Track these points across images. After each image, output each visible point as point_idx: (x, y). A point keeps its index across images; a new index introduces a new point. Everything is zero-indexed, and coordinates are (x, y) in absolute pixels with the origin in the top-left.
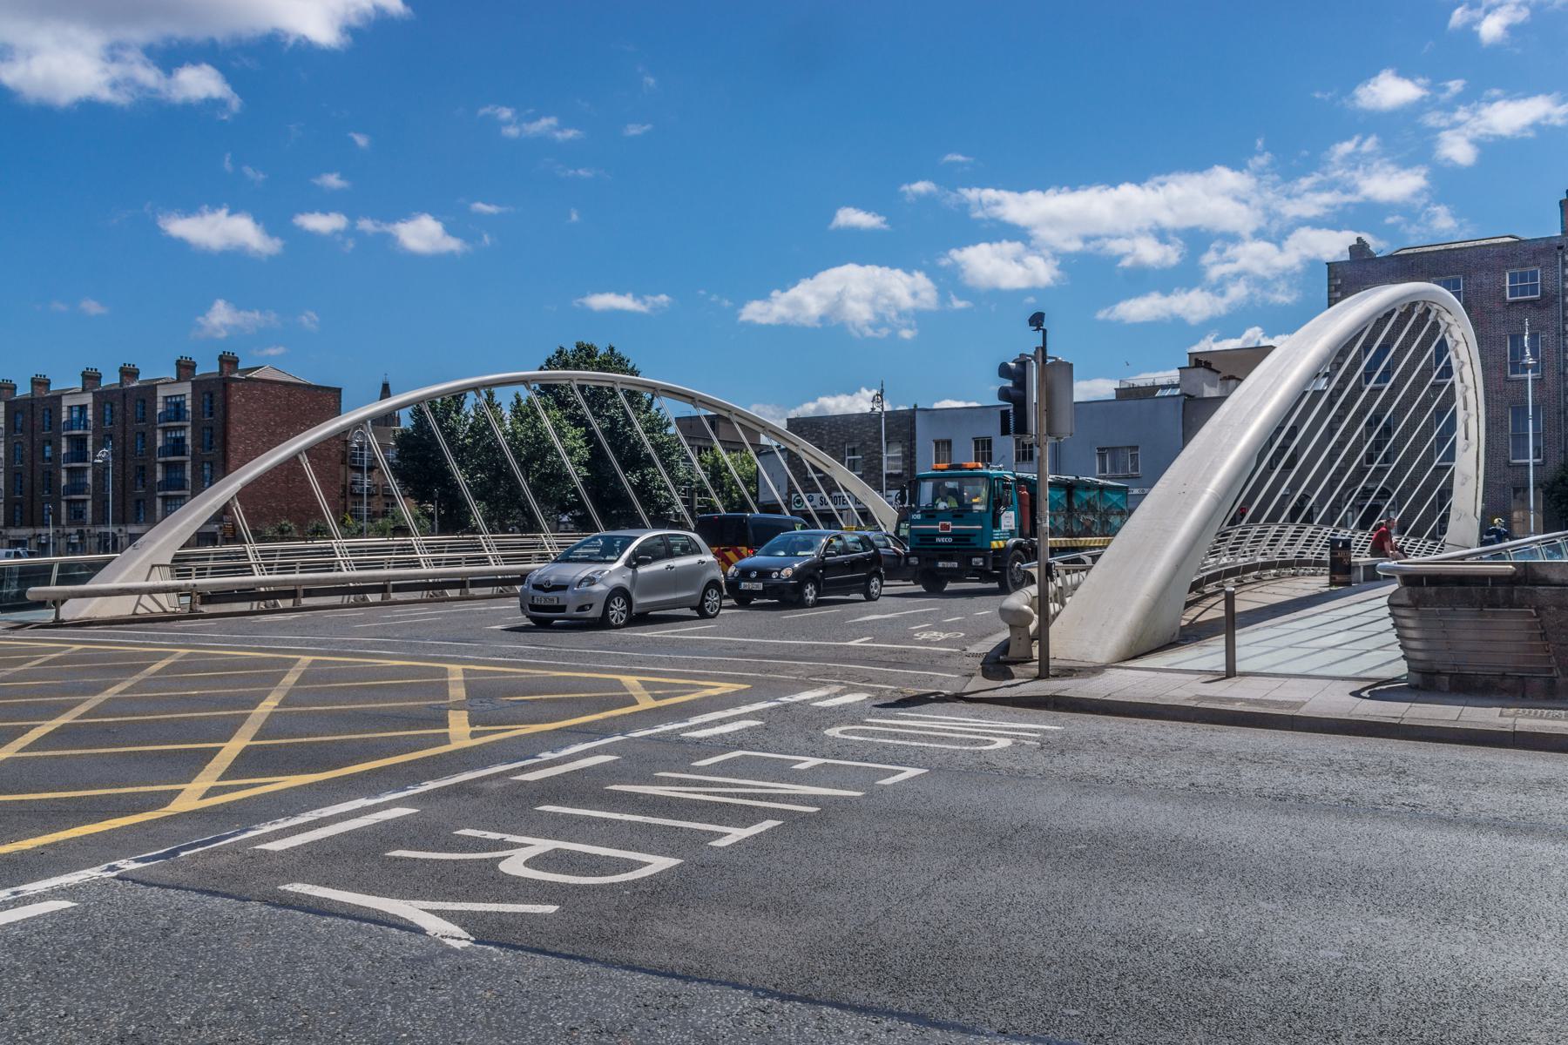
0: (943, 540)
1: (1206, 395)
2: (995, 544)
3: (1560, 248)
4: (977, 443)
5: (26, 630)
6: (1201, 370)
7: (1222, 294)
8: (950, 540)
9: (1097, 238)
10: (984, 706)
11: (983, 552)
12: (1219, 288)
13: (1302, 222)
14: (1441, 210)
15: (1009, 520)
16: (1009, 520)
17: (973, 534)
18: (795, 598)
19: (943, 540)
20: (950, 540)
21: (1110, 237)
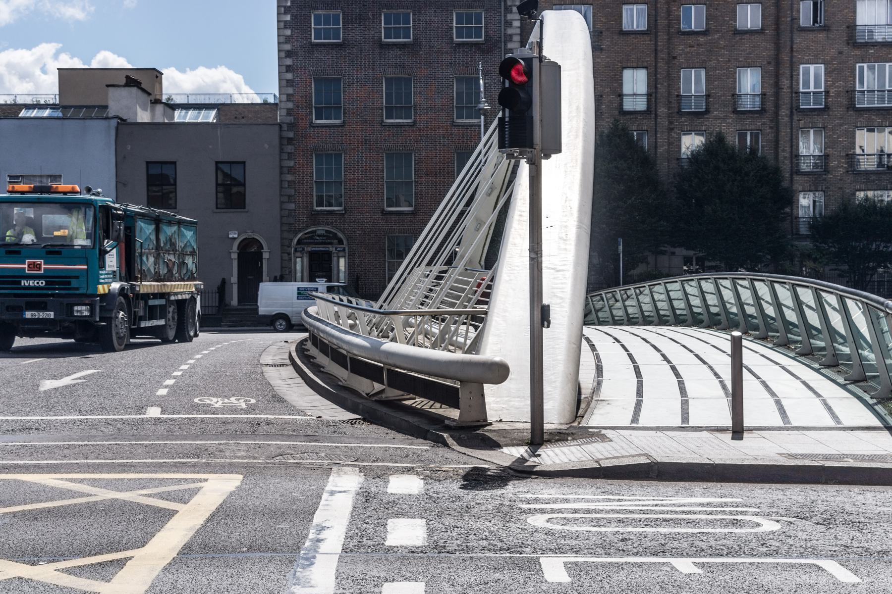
1: (139, 120)
2: (102, 289)
5: (34, 434)
6: (134, 90)
8: (42, 283)
10: (569, 480)
11: (89, 298)
15: (112, 261)
16: (112, 261)
17: (76, 276)
20: (42, 283)
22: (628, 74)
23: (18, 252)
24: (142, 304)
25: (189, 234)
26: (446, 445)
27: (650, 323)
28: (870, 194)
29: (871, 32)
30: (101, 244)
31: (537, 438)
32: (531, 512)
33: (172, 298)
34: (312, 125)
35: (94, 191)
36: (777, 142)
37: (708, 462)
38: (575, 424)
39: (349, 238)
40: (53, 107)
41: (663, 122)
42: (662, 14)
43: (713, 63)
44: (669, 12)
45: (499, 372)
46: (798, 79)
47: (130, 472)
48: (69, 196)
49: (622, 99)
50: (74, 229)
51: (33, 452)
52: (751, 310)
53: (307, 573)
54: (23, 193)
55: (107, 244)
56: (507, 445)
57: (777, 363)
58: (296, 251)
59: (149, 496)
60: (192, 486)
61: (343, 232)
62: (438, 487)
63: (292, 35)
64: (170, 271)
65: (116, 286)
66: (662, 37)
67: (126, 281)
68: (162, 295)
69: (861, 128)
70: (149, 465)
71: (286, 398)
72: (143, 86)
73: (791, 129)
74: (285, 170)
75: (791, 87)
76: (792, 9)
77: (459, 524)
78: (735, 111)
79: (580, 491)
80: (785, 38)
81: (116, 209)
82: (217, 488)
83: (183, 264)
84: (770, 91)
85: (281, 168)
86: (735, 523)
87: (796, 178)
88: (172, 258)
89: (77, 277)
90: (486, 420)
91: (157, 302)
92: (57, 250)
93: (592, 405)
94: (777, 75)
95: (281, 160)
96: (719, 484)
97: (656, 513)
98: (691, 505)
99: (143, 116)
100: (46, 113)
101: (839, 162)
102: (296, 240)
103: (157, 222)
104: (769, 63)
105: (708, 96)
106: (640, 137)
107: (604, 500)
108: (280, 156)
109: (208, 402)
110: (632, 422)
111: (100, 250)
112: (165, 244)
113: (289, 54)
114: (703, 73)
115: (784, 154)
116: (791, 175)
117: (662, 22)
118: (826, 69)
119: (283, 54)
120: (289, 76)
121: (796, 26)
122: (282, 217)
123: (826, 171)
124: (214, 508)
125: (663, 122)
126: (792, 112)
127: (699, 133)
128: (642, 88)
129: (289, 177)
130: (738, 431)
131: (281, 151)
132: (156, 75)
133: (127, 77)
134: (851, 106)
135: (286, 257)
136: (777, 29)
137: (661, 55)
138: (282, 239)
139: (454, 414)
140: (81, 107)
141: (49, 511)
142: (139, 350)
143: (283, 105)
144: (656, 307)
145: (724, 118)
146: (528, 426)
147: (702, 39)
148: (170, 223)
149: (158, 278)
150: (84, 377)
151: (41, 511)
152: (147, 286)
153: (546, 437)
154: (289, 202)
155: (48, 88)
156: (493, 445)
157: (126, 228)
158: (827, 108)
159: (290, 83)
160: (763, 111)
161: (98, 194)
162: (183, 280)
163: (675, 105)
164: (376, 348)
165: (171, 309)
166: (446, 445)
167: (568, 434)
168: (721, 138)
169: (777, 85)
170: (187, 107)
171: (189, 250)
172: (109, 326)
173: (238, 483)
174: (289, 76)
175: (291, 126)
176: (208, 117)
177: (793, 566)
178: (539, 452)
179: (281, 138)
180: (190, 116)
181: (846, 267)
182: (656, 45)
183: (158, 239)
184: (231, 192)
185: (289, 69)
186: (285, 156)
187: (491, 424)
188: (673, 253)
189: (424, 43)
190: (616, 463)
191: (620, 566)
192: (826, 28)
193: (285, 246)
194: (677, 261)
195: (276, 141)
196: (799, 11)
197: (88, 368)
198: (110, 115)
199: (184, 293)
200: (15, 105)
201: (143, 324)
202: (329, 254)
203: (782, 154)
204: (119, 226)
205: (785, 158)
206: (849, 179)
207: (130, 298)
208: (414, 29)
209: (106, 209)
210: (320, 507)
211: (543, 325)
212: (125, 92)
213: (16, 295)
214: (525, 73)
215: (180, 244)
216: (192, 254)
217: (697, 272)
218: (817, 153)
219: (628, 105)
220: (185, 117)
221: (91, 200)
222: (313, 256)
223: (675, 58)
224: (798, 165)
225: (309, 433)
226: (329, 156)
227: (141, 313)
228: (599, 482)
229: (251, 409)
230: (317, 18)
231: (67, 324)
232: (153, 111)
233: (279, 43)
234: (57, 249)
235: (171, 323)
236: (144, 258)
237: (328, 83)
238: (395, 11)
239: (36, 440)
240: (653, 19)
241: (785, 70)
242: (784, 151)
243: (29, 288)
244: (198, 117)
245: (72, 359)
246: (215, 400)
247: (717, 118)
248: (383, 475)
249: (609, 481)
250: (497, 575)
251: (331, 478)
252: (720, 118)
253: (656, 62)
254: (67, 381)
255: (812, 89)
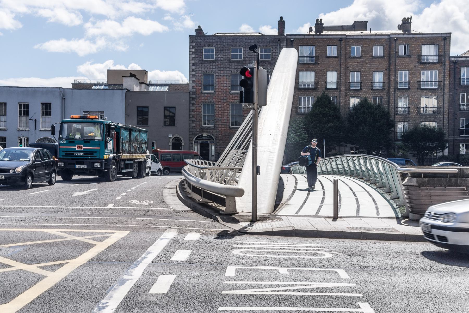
0: (78, 154)
1: (135, 90)
2: (105, 157)
3: (279, 40)
4: (20, 105)
5: (59, 213)
6: (133, 78)
7: (94, 43)
8: (82, 154)
9: (35, 7)
10: (259, 236)
11: (100, 160)
12: (93, 40)
13: (131, 14)
14: (188, 18)
15: (110, 146)
16: (110, 146)
17: (95, 151)
18: (23, 183)
19: (78, 154)
20: (82, 154)
21: (40, 8)
22: (329, 74)
23: (73, 142)
24: (122, 163)
25: (144, 135)
26: (218, 221)
27: (324, 174)
28: (427, 123)
29: (427, 58)
30: (106, 139)
31: (254, 219)
32: (236, 248)
33: (136, 161)
34: (202, 93)
35: (104, 118)
36: (389, 101)
37: (316, 230)
38: (273, 214)
39: (216, 138)
40: (105, 85)
41: (343, 93)
42: (343, 50)
43: (363, 70)
44: (346, 49)
45: (241, 193)
46: (398, 77)
47: (87, 229)
48: (94, 120)
49: (326, 84)
50: (96, 133)
51: (55, 220)
52: (352, 169)
53: (133, 270)
54: (76, 119)
55: (108, 139)
56: (242, 222)
57: (367, 191)
58: (195, 142)
59: (89, 239)
60: (108, 235)
61: (214, 135)
62: (206, 238)
63: (195, 57)
64: (135, 150)
65: (111, 156)
66: (343, 59)
67: (116, 154)
68: (131, 160)
69: (423, 96)
70: (95, 227)
71: (166, 201)
72: (137, 77)
73: (395, 96)
74: (191, 110)
75: (395, 80)
76: (395, 48)
77: (205, 253)
78: (372, 89)
79: (261, 240)
80: (393, 60)
81: (112, 125)
82: (117, 236)
83: (141, 147)
84: (386, 81)
85: (190, 109)
86: (315, 254)
87: (396, 116)
88: (136, 145)
89: (96, 152)
90: (236, 211)
91: (129, 162)
92: (88, 141)
93: (283, 206)
94: (389, 75)
95: (190, 106)
96: (319, 239)
97: (286, 249)
98: (302, 247)
99: (136, 89)
100: (102, 87)
101: (414, 110)
102: (195, 138)
103: (130, 130)
104: (386, 70)
105: (361, 83)
106: (333, 99)
107: (268, 244)
108: (189, 105)
109: (134, 202)
110: (316, 214)
111: (105, 141)
112: (133, 139)
113: (194, 64)
114: (359, 73)
115: (392, 107)
116: (395, 115)
117: (343, 53)
118: (409, 73)
119: (191, 64)
120: (194, 73)
121: (397, 55)
122: (189, 129)
123: (409, 113)
124: (111, 244)
125: (343, 93)
126: (395, 90)
127: (357, 97)
128: (335, 79)
129: (193, 113)
130: (335, 217)
131: (190, 102)
132: (145, 72)
133: (131, 73)
134: (419, 88)
135: (191, 145)
136: (390, 57)
137: (342, 66)
138: (189, 138)
139: (224, 208)
140: (116, 85)
141: (47, 244)
142: (123, 181)
143: (191, 85)
144: (332, 167)
145: (368, 91)
146: (251, 214)
147: (359, 60)
148: (136, 131)
149: (130, 153)
150: (92, 192)
151: (43, 244)
152: (124, 156)
153: (258, 219)
154: (193, 123)
155: (103, 78)
156: (237, 221)
157: (117, 133)
158: (409, 88)
159: (194, 76)
160: (383, 89)
161: (105, 119)
162: (141, 154)
163: (348, 86)
164: (198, 182)
165: (135, 165)
166: (218, 221)
167: (267, 218)
168: (366, 100)
169: (389, 79)
170: (157, 85)
171: (144, 142)
172: (108, 172)
173: (126, 234)
174: (194, 73)
175: (194, 93)
176: (165, 89)
177: (326, 271)
178: (254, 225)
179: (190, 98)
180: (158, 89)
181: (416, 153)
182: (340, 62)
183: (130, 137)
184: (170, 119)
185: (193, 70)
186: (191, 105)
187: (238, 213)
188: (346, 146)
189: (247, 60)
190: (279, 229)
191: (257, 270)
192: (409, 56)
193: (190, 141)
194: (347, 149)
195: (188, 99)
196: (398, 49)
197: (96, 188)
198: (123, 88)
199: (141, 159)
200: (91, 84)
201: (123, 171)
202: (208, 144)
203: (391, 107)
204: (114, 133)
205: (392, 108)
206: (418, 117)
207: (117, 161)
208: (244, 55)
209: (108, 125)
210: (153, 245)
211: (257, 174)
212: (129, 79)
213: (72, 159)
214: (250, 74)
215: (140, 139)
216: (145, 143)
217: (356, 153)
218: (405, 106)
219: (329, 86)
220: (156, 89)
221: (102, 122)
222: (201, 145)
223: (348, 67)
224: (397, 111)
225: (167, 215)
226: (208, 105)
227: (122, 167)
228: (271, 237)
229: (150, 205)
230: (205, 50)
231: (92, 170)
232: (141, 86)
233: (190, 60)
234: (88, 141)
235: (135, 170)
236: (124, 145)
237: (209, 76)
238: (236, 48)
239: (58, 216)
240: (339, 51)
241: (393, 73)
242: (392, 105)
243: (78, 156)
244: (161, 89)
245: (92, 184)
246: (137, 201)
247: (365, 92)
248: (185, 233)
249: (275, 237)
250: (207, 273)
251: (165, 233)
252: (366, 92)
253: (340, 69)
254: (85, 193)
255: (403, 81)
